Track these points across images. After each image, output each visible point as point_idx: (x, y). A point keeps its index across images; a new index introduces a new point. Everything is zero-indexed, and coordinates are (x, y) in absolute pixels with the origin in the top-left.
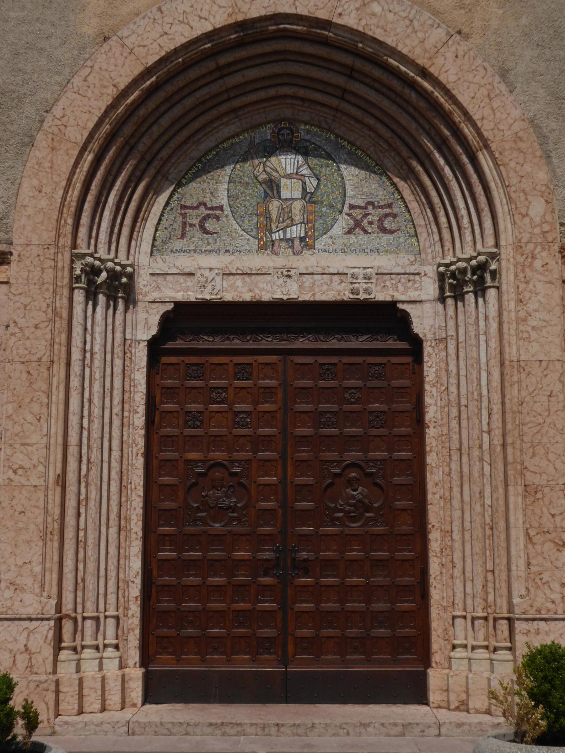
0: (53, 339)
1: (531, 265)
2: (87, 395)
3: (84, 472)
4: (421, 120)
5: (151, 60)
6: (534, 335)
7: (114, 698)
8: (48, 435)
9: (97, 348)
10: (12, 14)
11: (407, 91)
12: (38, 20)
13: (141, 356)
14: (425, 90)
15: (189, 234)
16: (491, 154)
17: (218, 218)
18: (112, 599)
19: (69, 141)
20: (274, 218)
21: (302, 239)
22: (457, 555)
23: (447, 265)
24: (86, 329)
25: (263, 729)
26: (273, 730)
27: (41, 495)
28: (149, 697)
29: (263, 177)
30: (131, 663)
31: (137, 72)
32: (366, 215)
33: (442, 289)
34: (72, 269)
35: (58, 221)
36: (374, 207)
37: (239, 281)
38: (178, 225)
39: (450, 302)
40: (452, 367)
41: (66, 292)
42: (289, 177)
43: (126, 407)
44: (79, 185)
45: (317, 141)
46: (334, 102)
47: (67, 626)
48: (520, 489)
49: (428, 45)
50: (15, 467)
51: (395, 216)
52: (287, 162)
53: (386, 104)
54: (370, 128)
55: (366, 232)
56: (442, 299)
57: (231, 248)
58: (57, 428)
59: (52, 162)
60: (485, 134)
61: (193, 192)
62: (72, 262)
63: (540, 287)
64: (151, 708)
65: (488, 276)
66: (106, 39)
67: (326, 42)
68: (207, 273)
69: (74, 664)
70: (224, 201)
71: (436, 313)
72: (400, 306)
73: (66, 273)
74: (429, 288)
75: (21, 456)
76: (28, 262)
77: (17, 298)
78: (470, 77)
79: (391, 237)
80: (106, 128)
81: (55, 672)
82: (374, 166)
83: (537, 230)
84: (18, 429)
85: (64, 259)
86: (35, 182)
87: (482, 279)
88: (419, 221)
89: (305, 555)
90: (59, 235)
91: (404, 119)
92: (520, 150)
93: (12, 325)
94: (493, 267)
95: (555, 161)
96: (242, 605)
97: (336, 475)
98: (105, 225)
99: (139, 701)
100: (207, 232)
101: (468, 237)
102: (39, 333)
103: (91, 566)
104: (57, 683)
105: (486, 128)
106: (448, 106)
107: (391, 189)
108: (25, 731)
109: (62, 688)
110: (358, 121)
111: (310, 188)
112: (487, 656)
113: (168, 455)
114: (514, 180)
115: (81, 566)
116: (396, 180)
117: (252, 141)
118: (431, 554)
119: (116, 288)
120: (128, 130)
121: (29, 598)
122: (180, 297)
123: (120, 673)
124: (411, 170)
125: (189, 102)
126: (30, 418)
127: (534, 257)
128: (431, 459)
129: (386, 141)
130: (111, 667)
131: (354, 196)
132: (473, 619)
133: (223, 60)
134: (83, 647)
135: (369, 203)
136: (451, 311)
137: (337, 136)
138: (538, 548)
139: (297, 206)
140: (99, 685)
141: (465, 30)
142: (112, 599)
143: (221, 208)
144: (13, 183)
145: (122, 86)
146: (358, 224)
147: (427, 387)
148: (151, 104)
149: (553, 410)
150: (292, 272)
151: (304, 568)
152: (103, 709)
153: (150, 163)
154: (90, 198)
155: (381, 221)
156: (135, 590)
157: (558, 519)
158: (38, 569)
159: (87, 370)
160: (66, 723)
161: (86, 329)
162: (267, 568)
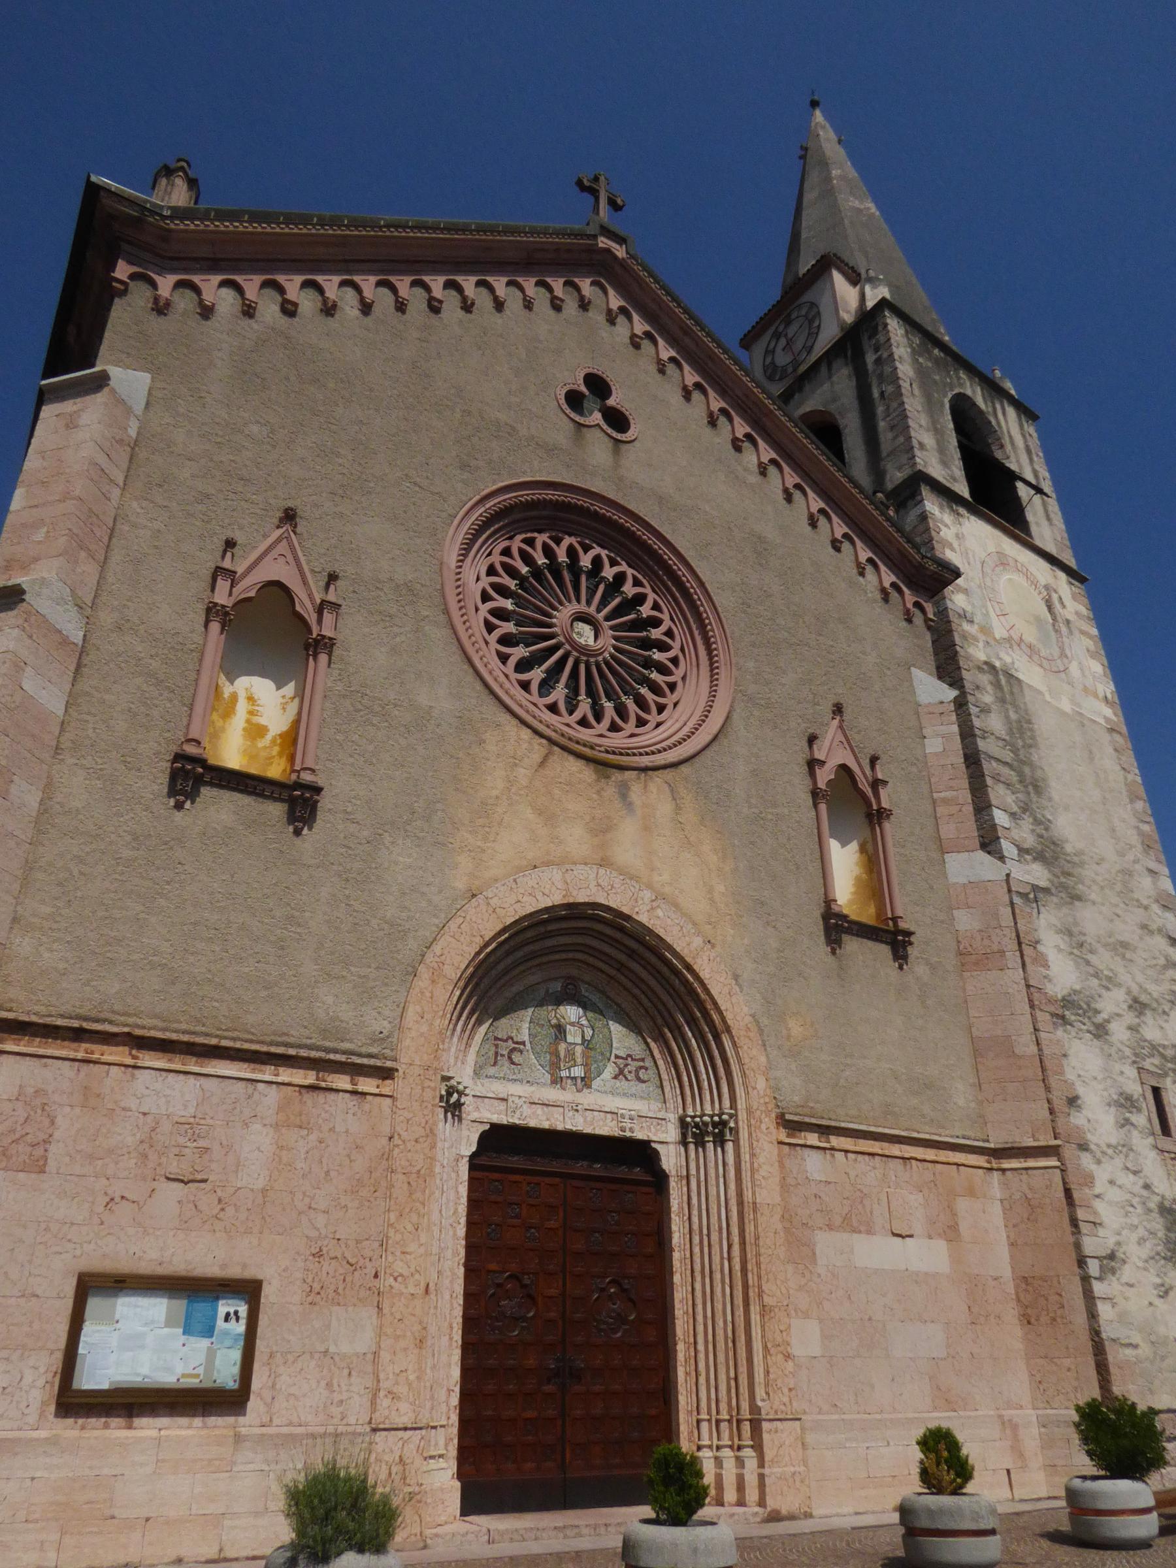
4: (678, 1001)
11: (673, 977)
14: (687, 981)
15: (500, 1063)
16: (732, 1037)
17: (521, 1052)
19: (445, 976)
21: (583, 1079)
26: (603, 1529)
29: (554, 1021)
31: (498, 929)
32: (626, 1065)
33: (684, 1135)
36: (633, 1060)
37: (539, 1110)
39: (692, 1147)
42: (572, 1024)
46: (613, 972)
50: (396, 1274)
51: (646, 1069)
52: (571, 1012)
53: (653, 983)
55: (626, 1079)
59: (432, 992)
61: (505, 1026)
66: (474, 896)
67: (622, 929)
68: (517, 1100)
70: (526, 1038)
72: (653, 1145)
74: (672, 1133)
75: (401, 1264)
76: (411, 1080)
77: (401, 1112)
79: (644, 1085)
80: (471, 969)
82: (634, 1027)
83: (762, 1101)
84: (398, 1237)
87: (722, 1134)
88: (665, 1076)
93: (396, 1137)
94: (732, 1125)
96: (530, 1414)
100: (513, 1063)
102: (418, 1146)
105: (729, 1016)
106: (703, 996)
107: (644, 1046)
110: (626, 989)
112: (732, 1454)
116: (649, 1040)
122: (495, 1119)
124: (663, 1036)
126: (410, 1227)
129: (646, 1010)
132: (718, 1422)
135: (629, 1056)
139: (579, 1050)
143: (523, 1043)
144: (398, 1006)
146: (621, 1072)
147: (673, 1216)
150: (579, 1108)
155: (637, 1071)
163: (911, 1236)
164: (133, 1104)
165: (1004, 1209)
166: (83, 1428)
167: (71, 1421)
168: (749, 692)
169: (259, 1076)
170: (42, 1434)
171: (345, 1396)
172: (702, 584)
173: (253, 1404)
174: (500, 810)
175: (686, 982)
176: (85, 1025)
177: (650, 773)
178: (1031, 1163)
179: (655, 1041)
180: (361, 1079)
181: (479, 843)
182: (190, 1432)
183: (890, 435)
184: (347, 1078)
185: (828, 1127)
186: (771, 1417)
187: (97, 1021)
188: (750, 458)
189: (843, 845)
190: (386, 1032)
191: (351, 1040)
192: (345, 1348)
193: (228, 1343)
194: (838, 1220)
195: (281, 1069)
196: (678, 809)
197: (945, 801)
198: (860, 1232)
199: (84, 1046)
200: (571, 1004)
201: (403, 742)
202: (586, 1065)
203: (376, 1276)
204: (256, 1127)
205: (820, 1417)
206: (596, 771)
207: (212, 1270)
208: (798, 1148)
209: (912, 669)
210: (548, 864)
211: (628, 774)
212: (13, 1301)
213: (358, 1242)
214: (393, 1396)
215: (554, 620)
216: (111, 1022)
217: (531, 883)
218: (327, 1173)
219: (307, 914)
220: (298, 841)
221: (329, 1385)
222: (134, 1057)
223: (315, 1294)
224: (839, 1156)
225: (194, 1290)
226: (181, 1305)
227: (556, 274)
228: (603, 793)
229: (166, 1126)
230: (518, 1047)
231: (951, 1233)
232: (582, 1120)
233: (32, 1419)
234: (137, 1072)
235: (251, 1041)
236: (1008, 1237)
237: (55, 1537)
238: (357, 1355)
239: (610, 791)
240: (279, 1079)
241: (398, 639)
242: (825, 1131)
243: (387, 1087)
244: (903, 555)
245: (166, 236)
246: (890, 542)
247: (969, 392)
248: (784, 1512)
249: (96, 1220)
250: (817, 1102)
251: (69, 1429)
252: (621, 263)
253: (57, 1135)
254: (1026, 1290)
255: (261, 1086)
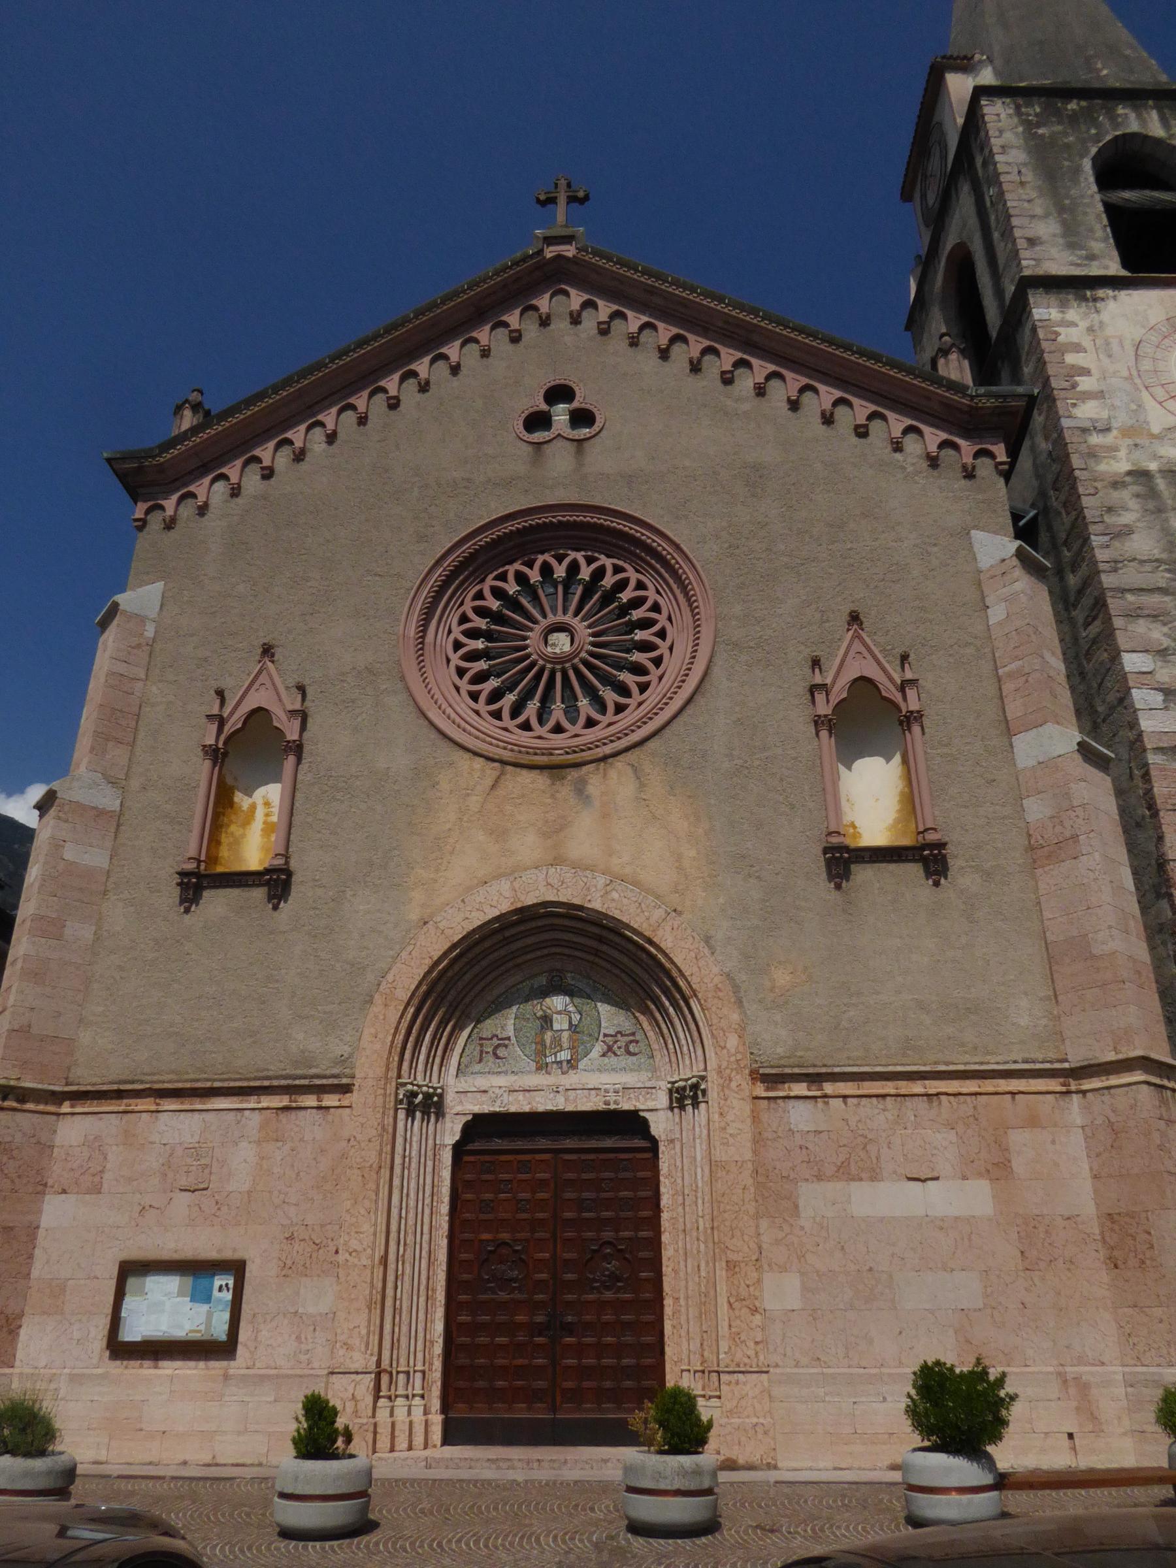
0: (381, 1150)
1: (728, 1087)
2: (405, 1191)
3: (401, 1252)
5: (456, 938)
6: (731, 1140)
7: (419, 1440)
8: (375, 1225)
9: (414, 1153)
10: (361, 907)
11: (639, 953)
12: (379, 911)
13: (447, 1157)
17: (506, 1046)
18: (420, 1356)
20: (548, 1045)
21: (568, 1062)
22: (683, 1318)
23: (673, 1083)
24: (406, 1140)
25: (528, 1463)
26: (536, 1465)
27: (368, 1272)
28: (447, 1440)
29: (540, 1013)
30: (433, 1410)
32: (616, 1042)
34: (397, 1094)
35: (388, 1059)
36: (622, 1035)
37: (520, 1096)
38: (476, 1053)
39: (676, 1110)
40: (679, 1163)
41: (392, 1112)
42: (559, 1013)
43: (435, 1198)
44: (403, 1031)
45: (580, 985)
46: (591, 958)
47: (385, 1378)
48: (724, 1264)
49: (652, 921)
51: (637, 1042)
52: (558, 1002)
53: (625, 960)
54: (617, 976)
55: (616, 1055)
56: (671, 1108)
57: (515, 1070)
58: (382, 1219)
60: (694, 986)
61: (489, 1027)
62: (397, 1088)
63: (735, 1103)
64: (447, 1448)
65: (699, 1093)
66: (425, 923)
68: (497, 1091)
69: (388, 1410)
71: (667, 1119)
72: (642, 1114)
73: (393, 1098)
78: (682, 944)
79: (634, 1058)
80: (424, 988)
81: (374, 1416)
82: (621, 1003)
83: (733, 1059)
85: (391, 1088)
86: (373, 1031)
88: (655, 1046)
89: (570, 1319)
90: (388, 1069)
91: (638, 970)
92: (719, 998)
94: (703, 1087)
95: (745, 1004)
96: (520, 1362)
97: (594, 1251)
98: (422, 1057)
99: (439, 1443)
100: (498, 1057)
101: (687, 1062)
103: (404, 1329)
104: (375, 1425)
105: (694, 981)
106: (668, 965)
107: (634, 1021)
108: (236, 799)
109: (379, 1430)
111: (575, 1022)
113: (466, 1236)
114: (715, 1021)
115: (397, 1330)
116: (638, 1014)
117: (532, 987)
118: (665, 1317)
119: (429, 1106)
120: (439, 987)
121: (357, 1355)
122: (477, 1109)
123: (423, 1418)
124: (648, 1007)
125: (484, 963)
126: (363, 1211)
127: (731, 1080)
128: (665, 1238)
130: (418, 1413)
131: (607, 1027)
133: (507, 934)
134: (396, 1396)
136: (677, 1119)
137: (595, 981)
138: (737, 1312)
139: (566, 1035)
140: (407, 1427)
141: (679, 909)
142: (420, 1356)
143: (509, 1039)
145: (435, 958)
146: (610, 1049)
147: (662, 1178)
148: (456, 968)
149: (746, 1200)
151: (569, 1329)
152: (410, 1448)
153: (457, 1007)
154: (411, 1039)
155: (627, 1046)
156: (438, 1349)
157: (752, 1289)
158: (364, 1332)
159: (406, 1172)
160: (380, 1458)
161: (406, 1140)
162: (540, 1330)
163: (937, 1179)
164: (155, 1137)
165: (1086, 1138)
166: (126, 1367)
167: (118, 1363)
168: (734, 639)
169: (244, 1106)
170: (100, 1371)
171: (310, 1346)
172: (677, 547)
173: (240, 1350)
174: (451, 840)
175: (649, 954)
176: (122, 1087)
177: (610, 760)
178: (1114, 1081)
179: (643, 1013)
180: (326, 1096)
181: (432, 876)
182: (194, 1372)
183: (1002, 244)
184: (314, 1097)
185: (818, 1075)
186: (731, 1369)
187: (133, 1082)
188: (746, 382)
189: (888, 760)
190: (346, 1055)
191: (317, 1067)
192: (311, 1310)
193: (221, 1307)
194: (829, 1170)
195: (263, 1098)
196: (642, 786)
197: (1010, 675)
198: (861, 1180)
199: (125, 1101)
200: (557, 994)
201: (363, 806)
202: (574, 1047)
203: (337, 1252)
204: (244, 1144)
205: (796, 1370)
206: (552, 777)
207: (213, 1255)
208: (779, 1101)
209: (973, 532)
210: (498, 877)
211: (585, 769)
212: (82, 1282)
213: (322, 1226)
214: (348, 1347)
215: (528, 642)
216: (142, 1082)
217: (478, 899)
218: (298, 1174)
219: (283, 971)
220: (276, 914)
221: (298, 1338)
222: (158, 1104)
223: (288, 1270)
224: (836, 1103)
225: (196, 1270)
226: (189, 1281)
227: (509, 309)
228: (558, 795)
229: (179, 1152)
230: (504, 1042)
231: (999, 1170)
232: (563, 1099)
233: (95, 1361)
234: (160, 1115)
235: (235, 1080)
236: (1091, 1169)
237: (107, 1440)
238: (320, 1314)
239: (565, 790)
240: (260, 1106)
241: (359, 719)
242: (815, 1079)
243: (347, 1100)
244: (948, 405)
245: (161, 468)
246: (929, 399)
247: (1134, 126)
248: (741, 1461)
249: (133, 1223)
250: (809, 1049)
251: (117, 1368)
252: (574, 261)
253: (108, 1166)
254: (1112, 1230)
255: (247, 1113)
